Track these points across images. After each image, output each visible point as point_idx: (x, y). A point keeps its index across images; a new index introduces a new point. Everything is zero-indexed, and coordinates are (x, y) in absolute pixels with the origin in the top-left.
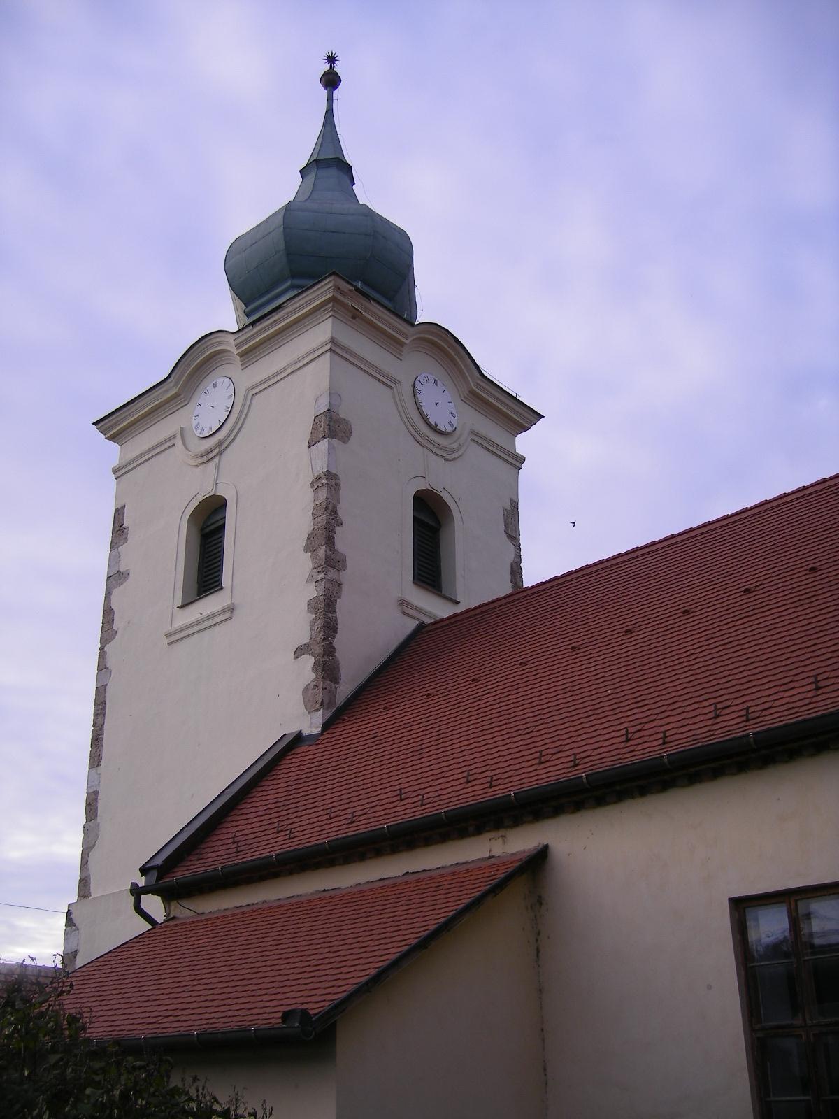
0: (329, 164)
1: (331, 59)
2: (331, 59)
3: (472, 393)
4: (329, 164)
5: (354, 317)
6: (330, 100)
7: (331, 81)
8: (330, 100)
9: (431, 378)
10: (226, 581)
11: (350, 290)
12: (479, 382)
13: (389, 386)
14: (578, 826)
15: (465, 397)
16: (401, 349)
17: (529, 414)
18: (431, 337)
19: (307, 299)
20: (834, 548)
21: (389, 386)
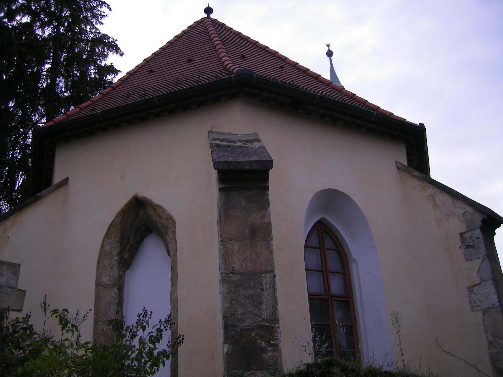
1: (328, 45)
6: (331, 61)
7: (330, 54)
8: (331, 61)
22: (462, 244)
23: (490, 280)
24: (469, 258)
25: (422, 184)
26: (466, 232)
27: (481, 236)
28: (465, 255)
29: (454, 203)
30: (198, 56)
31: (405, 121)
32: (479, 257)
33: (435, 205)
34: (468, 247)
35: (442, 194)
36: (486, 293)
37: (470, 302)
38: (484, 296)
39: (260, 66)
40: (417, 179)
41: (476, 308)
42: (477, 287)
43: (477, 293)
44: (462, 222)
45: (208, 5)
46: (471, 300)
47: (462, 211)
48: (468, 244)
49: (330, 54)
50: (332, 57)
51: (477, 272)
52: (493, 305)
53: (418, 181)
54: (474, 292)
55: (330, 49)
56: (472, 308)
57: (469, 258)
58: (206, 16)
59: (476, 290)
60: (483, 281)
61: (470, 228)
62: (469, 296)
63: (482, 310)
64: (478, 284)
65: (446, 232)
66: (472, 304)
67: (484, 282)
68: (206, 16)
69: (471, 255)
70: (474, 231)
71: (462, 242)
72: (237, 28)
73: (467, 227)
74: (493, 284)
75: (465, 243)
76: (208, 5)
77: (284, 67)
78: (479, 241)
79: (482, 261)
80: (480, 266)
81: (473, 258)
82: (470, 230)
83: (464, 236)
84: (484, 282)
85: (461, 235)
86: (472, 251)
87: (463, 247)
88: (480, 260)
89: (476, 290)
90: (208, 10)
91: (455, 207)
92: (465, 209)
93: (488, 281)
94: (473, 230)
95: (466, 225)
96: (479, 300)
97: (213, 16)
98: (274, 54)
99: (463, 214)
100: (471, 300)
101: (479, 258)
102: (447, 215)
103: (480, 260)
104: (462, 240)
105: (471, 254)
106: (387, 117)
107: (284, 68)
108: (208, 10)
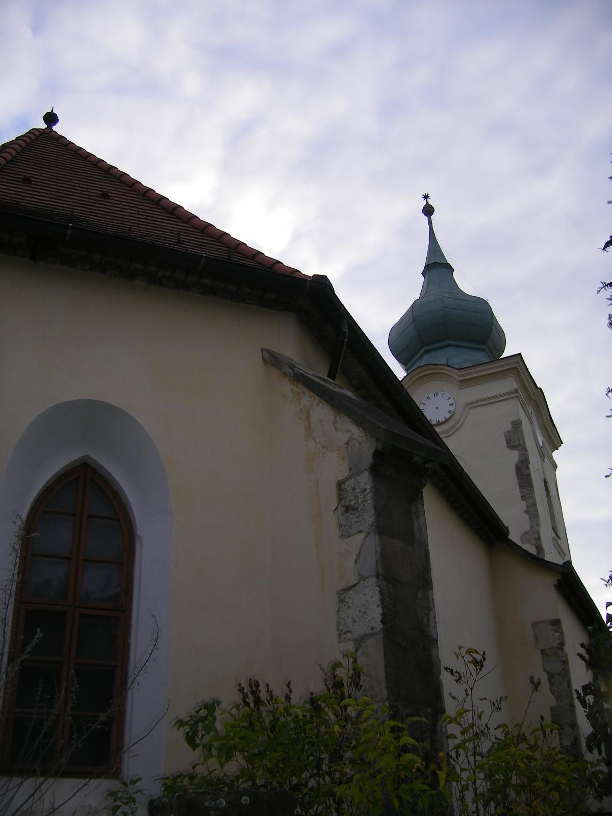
0: (437, 267)
1: (426, 197)
2: (426, 197)
3: (461, 381)
4: (437, 267)
6: (430, 223)
7: (428, 211)
8: (430, 223)
9: (431, 395)
12: (461, 374)
22: (338, 505)
23: (372, 577)
24: (346, 532)
25: (296, 389)
26: (347, 479)
27: (368, 487)
28: (341, 526)
29: (335, 422)
30: (12, 196)
31: (295, 275)
32: (361, 529)
33: (309, 429)
34: (348, 509)
35: (321, 405)
36: (364, 605)
37: (338, 624)
38: (360, 611)
39: (43, 194)
40: (290, 380)
41: (345, 636)
42: (351, 591)
43: (351, 605)
44: (343, 458)
45: (52, 110)
46: (339, 618)
47: (347, 437)
48: (347, 504)
49: (428, 211)
50: (432, 217)
51: (354, 561)
52: (372, 628)
53: (291, 384)
54: (345, 601)
55: (429, 203)
56: (340, 635)
57: (345, 534)
58: (43, 126)
59: (350, 598)
60: (363, 578)
61: (354, 473)
62: (338, 611)
63: (355, 640)
64: (354, 586)
65: (318, 480)
66: (341, 628)
67: (364, 581)
68: (43, 126)
69: (349, 526)
70: (358, 475)
71: (340, 499)
72: (79, 143)
73: (350, 469)
74: (377, 586)
75: (343, 503)
76: (52, 110)
77: (110, 194)
78: (365, 496)
79: (366, 537)
80: (362, 547)
81: (352, 532)
82: (354, 474)
83: (343, 487)
84: (363, 582)
85: (340, 484)
86: (353, 517)
87: (341, 509)
88: (362, 536)
89: (350, 598)
90: (51, 118)
91: (337, 430)
92: (350, 431)
93: (370, 578)
94: (357, 474)
95: (350, 465)
96: (352, 618)
97: (58, 128)
98: (118, 179)
99: (347, 444)
100: (339, 618)
101: (360, 532)
102: (323, 447)
103: (362, 536)
104: (340, 494)
105: (350, 524)
106: (288, 276)
107: (111, 198)
108: (51, 118)
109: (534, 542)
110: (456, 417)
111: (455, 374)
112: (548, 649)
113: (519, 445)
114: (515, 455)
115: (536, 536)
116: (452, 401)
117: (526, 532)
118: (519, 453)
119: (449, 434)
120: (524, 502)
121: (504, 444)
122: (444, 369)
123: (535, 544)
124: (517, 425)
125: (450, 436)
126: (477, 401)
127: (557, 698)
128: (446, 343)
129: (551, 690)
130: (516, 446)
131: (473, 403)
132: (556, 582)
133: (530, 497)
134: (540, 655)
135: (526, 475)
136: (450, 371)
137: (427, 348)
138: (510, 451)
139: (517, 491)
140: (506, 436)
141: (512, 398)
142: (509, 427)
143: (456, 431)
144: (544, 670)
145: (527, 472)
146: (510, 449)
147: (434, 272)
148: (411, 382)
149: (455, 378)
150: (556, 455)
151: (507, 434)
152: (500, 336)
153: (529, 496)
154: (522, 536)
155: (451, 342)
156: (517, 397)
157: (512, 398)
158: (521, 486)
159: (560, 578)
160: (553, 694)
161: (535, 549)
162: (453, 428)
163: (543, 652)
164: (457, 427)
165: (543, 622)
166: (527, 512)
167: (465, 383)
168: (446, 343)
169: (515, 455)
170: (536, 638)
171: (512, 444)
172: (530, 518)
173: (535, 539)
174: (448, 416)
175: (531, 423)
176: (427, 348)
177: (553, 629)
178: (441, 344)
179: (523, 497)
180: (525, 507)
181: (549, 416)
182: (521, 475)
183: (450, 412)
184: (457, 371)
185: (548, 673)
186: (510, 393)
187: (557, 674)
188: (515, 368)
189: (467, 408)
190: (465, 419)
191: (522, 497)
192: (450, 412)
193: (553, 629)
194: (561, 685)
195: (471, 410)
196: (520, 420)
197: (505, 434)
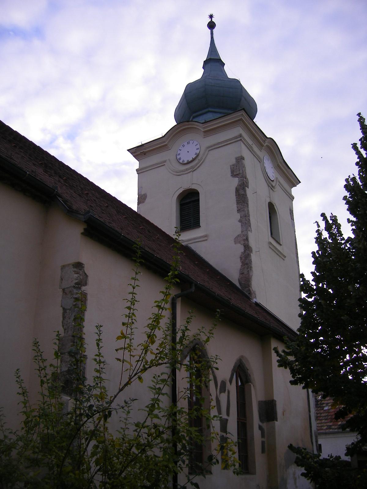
0: (213, 61)
1: (211, 16)
2: (211, 16)
3: (205, 132)
4: (213, 61)
5: (145, 154)
6: (212, 34)
7: (211, 26)
8: (212, 34)
9: (186, 144)
10: (201, 224)
11: (136, 150)
12: (204, 127)
13: (163, 165)
14: (248, 370)
15: (204, 136)
16: (168, 146)
17: (236, 114)
18: (180, 129)
19: (209, 125)
20: (189, 224)
21: (163, 165)
109: (242, 242)
110: (199, 157)
111: (201, 127)
112: (67, 288)
113: (239, 174)
114: (236, 181)
115: (245, 238)
116: (198, 146)
117: (238, 236)
118: (239, 180)
119: (194, 169)
120: (239, 214)
121: (229, 174)
122: (194, 125)
123: (244, 244)
124: (240, 159)
125: (194, 170)
126: (214, 145)
127: (65, 330)
128: (206, 110)
129: (62, 322)
130: (237, 174)
131: (211, 146)
132: (82, 231)
133: (244, 210)
134: (61, 293)
135: (242, 195)
136: (197, 126)
137: (194, 115)
138: (233, 178)
139: (234, 207)
140: (231, 168)
141: (238, 141)
142: (234, 161)
143: (199, 167)
144: (61, 306)
145: (243, 193)
146: (233, 177)
147: (209, 65)
148: (172, 135)
149: (200, 130)
150: (295, 191)
151: (232, 167)
152: (250, 105)
153: (243, 209)
154: (235, 239)
155: (210, 109)
156: (241, 140)
157: (238, 141)
158: (238, 202)
159: (85, 226)
160: (63, 326)
161: (243, 247)
162: (196, 165)
163: (64, 290)
164: (200, 164)
165: (69, 265)
166: (240, 221)
167: (207, 133)
168: (206, 110)
169: (236, 181)
170: (62, 279)
171: (235, 174)
172: (242, 225)
173: (244, 240)
174: (194, 156)
175: (260, 162)
176: (194, 115)
177: (74, 271)
178: (201, 112)
179: (239, 211)
180: (239, 218)
181: (282, 160)
182: (239, 195)
183: (196, 154)
184: (201, 125)
185: (64, 309)
186: (236, 137)
187: (68, 309)
188: (241, 120)
189: (207, 151)
190: (205, 158)
191: (238, 210)
192: (196, 154)
193: (74, 271)
194: (70, 318)
195: (211, 152)
196: (241, 156)
197: (231, 167)
